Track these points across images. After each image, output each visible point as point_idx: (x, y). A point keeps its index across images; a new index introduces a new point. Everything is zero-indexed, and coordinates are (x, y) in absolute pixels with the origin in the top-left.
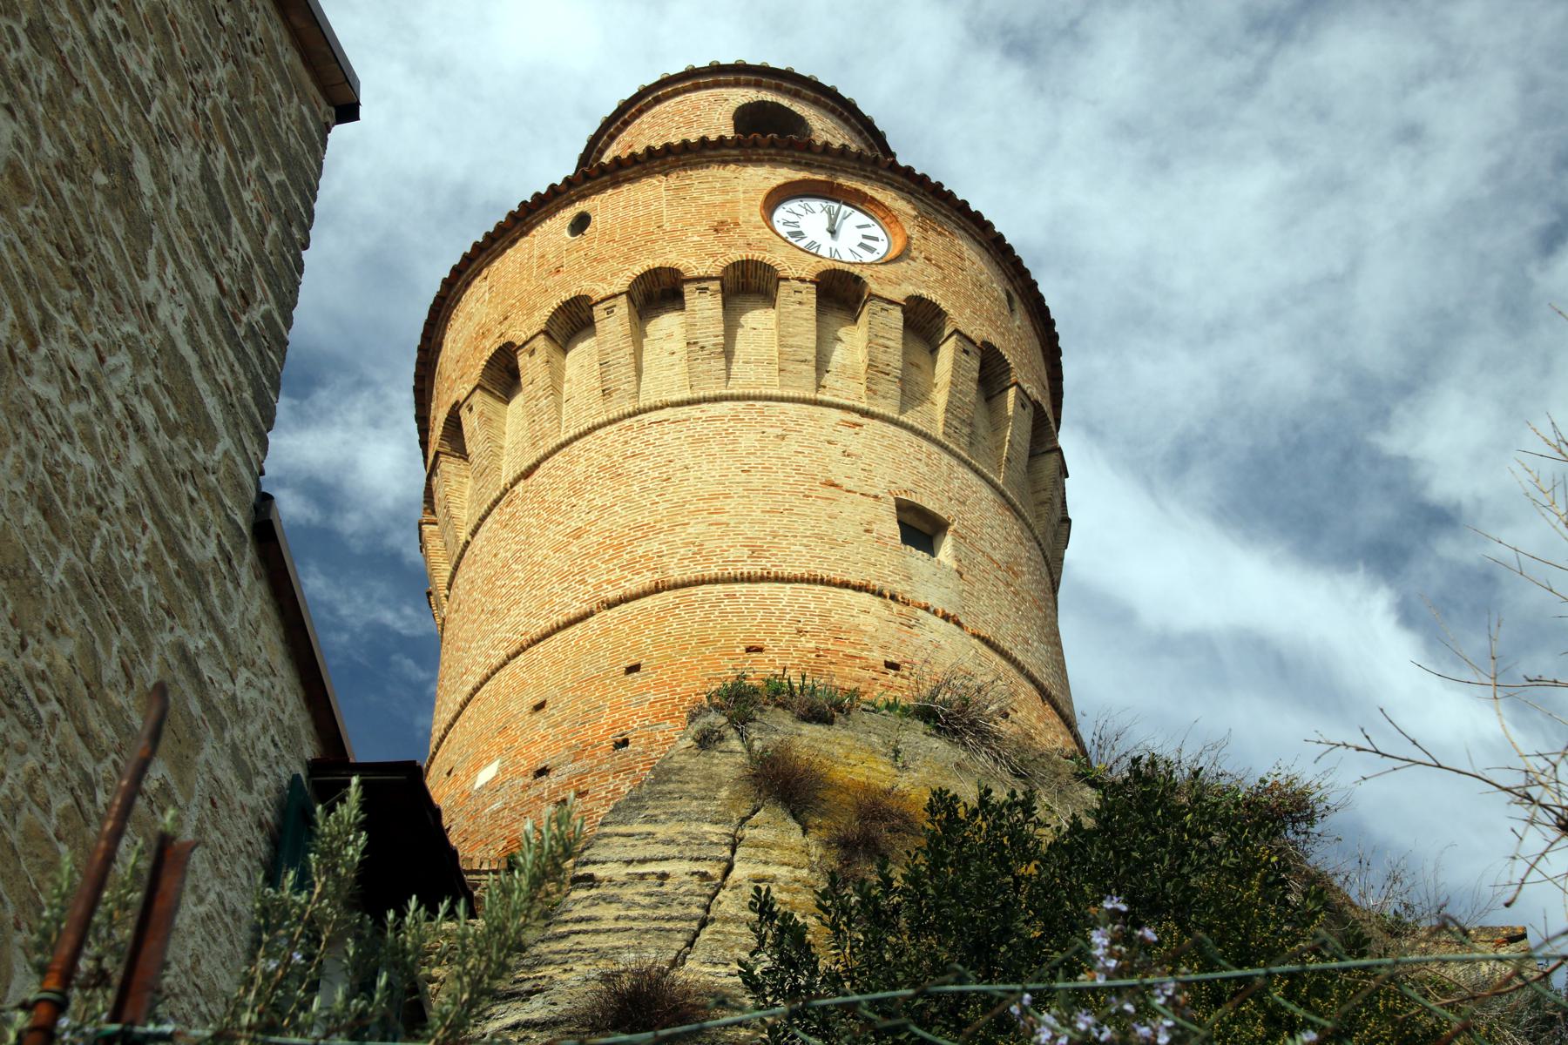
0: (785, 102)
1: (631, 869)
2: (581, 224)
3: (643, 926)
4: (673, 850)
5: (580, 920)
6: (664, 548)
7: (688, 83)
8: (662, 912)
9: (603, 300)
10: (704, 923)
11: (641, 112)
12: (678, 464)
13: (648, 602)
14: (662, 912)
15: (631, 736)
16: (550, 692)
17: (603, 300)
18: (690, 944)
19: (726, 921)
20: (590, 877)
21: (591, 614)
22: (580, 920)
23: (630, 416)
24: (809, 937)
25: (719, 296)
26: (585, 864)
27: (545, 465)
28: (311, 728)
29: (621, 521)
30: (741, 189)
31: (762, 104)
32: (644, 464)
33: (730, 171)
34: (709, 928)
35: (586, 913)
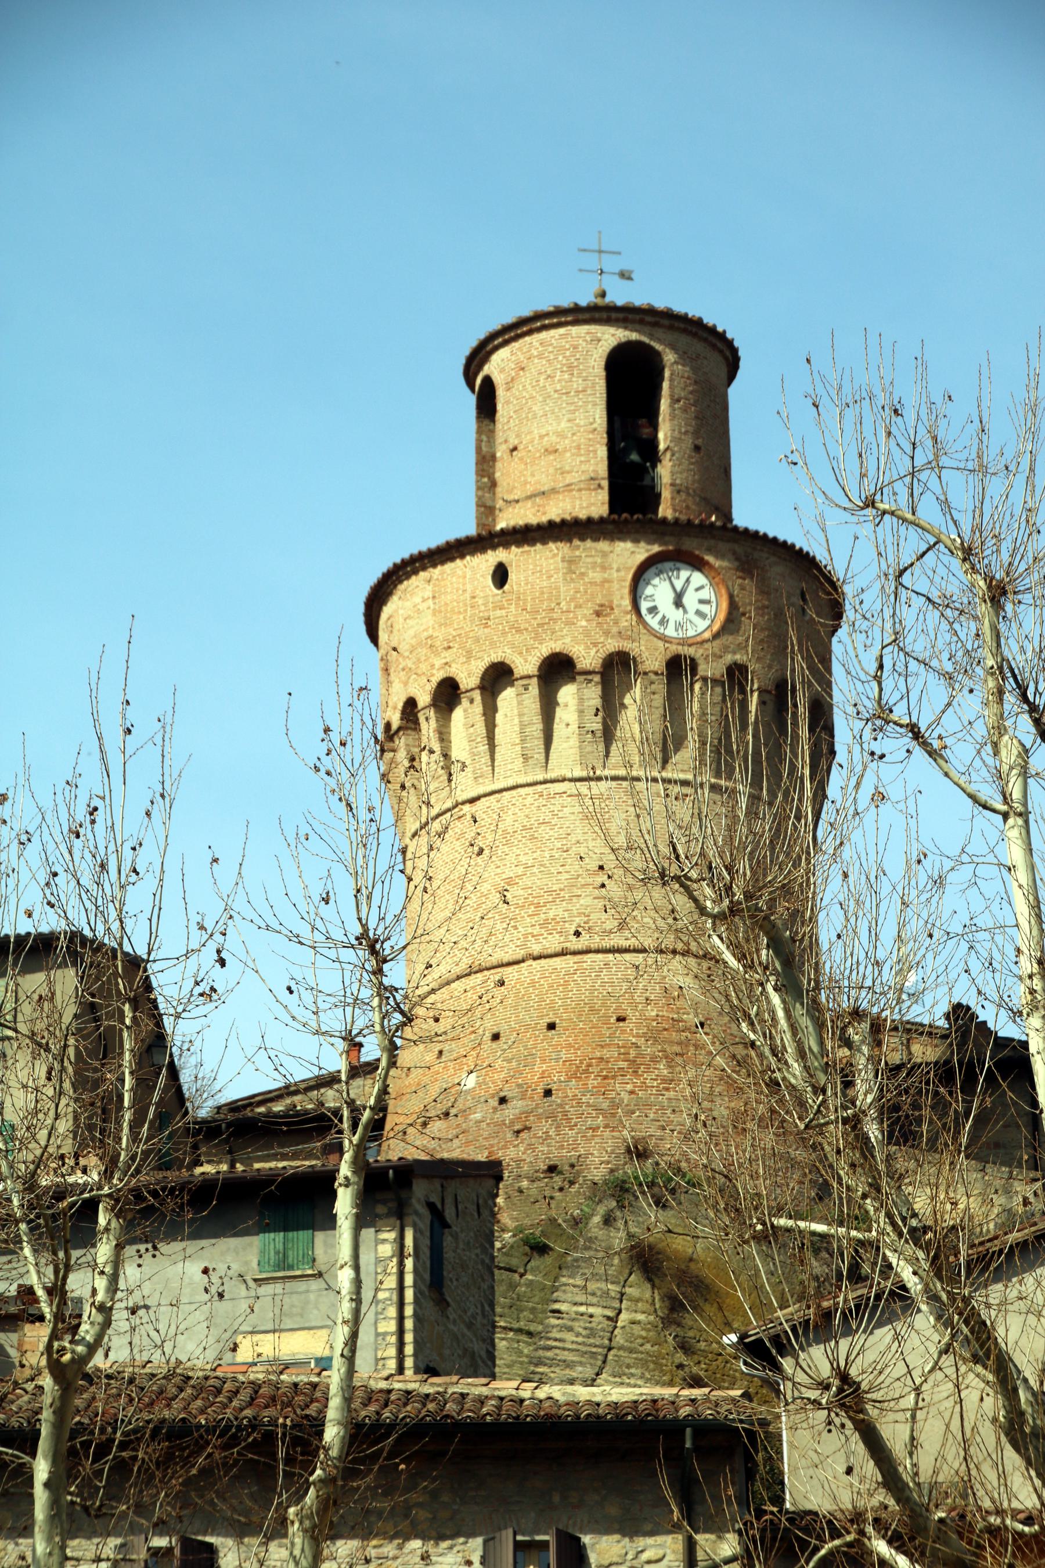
0: (653, 344)
1: (575, 1308)
2: (501, 575)
3: (584, 1349)
4: (595, 1300)
5: (556, 1340)
6: (566, 914)
7: (569, 319)
8: (592, 1341)
9: (522, 678)
10: (610, 1349)
11: (530, 332)
12: (573, 838)
13: (557, 961)
14: (592, 1341)
15: (554, 1087)
16: (503, 1029)
17: (522, 678)
18: (604, 1362)
19: (619, 1349)
20: (558, 1311)
21: (523, 961)
22: (556, 1340)
23: (541, 783)
24: (697, 522)
25: (600, 687)
26: (556, 1301)
27: (483, 800)
28: (527, 1410)
29: (539, 883)
30: (615, 566)
31: (638, 344)
32: (551, 833)
33: (603, 545)
34: (612, 1352)
35: (558, 1336)
